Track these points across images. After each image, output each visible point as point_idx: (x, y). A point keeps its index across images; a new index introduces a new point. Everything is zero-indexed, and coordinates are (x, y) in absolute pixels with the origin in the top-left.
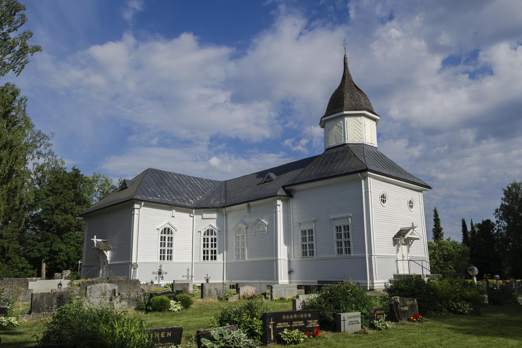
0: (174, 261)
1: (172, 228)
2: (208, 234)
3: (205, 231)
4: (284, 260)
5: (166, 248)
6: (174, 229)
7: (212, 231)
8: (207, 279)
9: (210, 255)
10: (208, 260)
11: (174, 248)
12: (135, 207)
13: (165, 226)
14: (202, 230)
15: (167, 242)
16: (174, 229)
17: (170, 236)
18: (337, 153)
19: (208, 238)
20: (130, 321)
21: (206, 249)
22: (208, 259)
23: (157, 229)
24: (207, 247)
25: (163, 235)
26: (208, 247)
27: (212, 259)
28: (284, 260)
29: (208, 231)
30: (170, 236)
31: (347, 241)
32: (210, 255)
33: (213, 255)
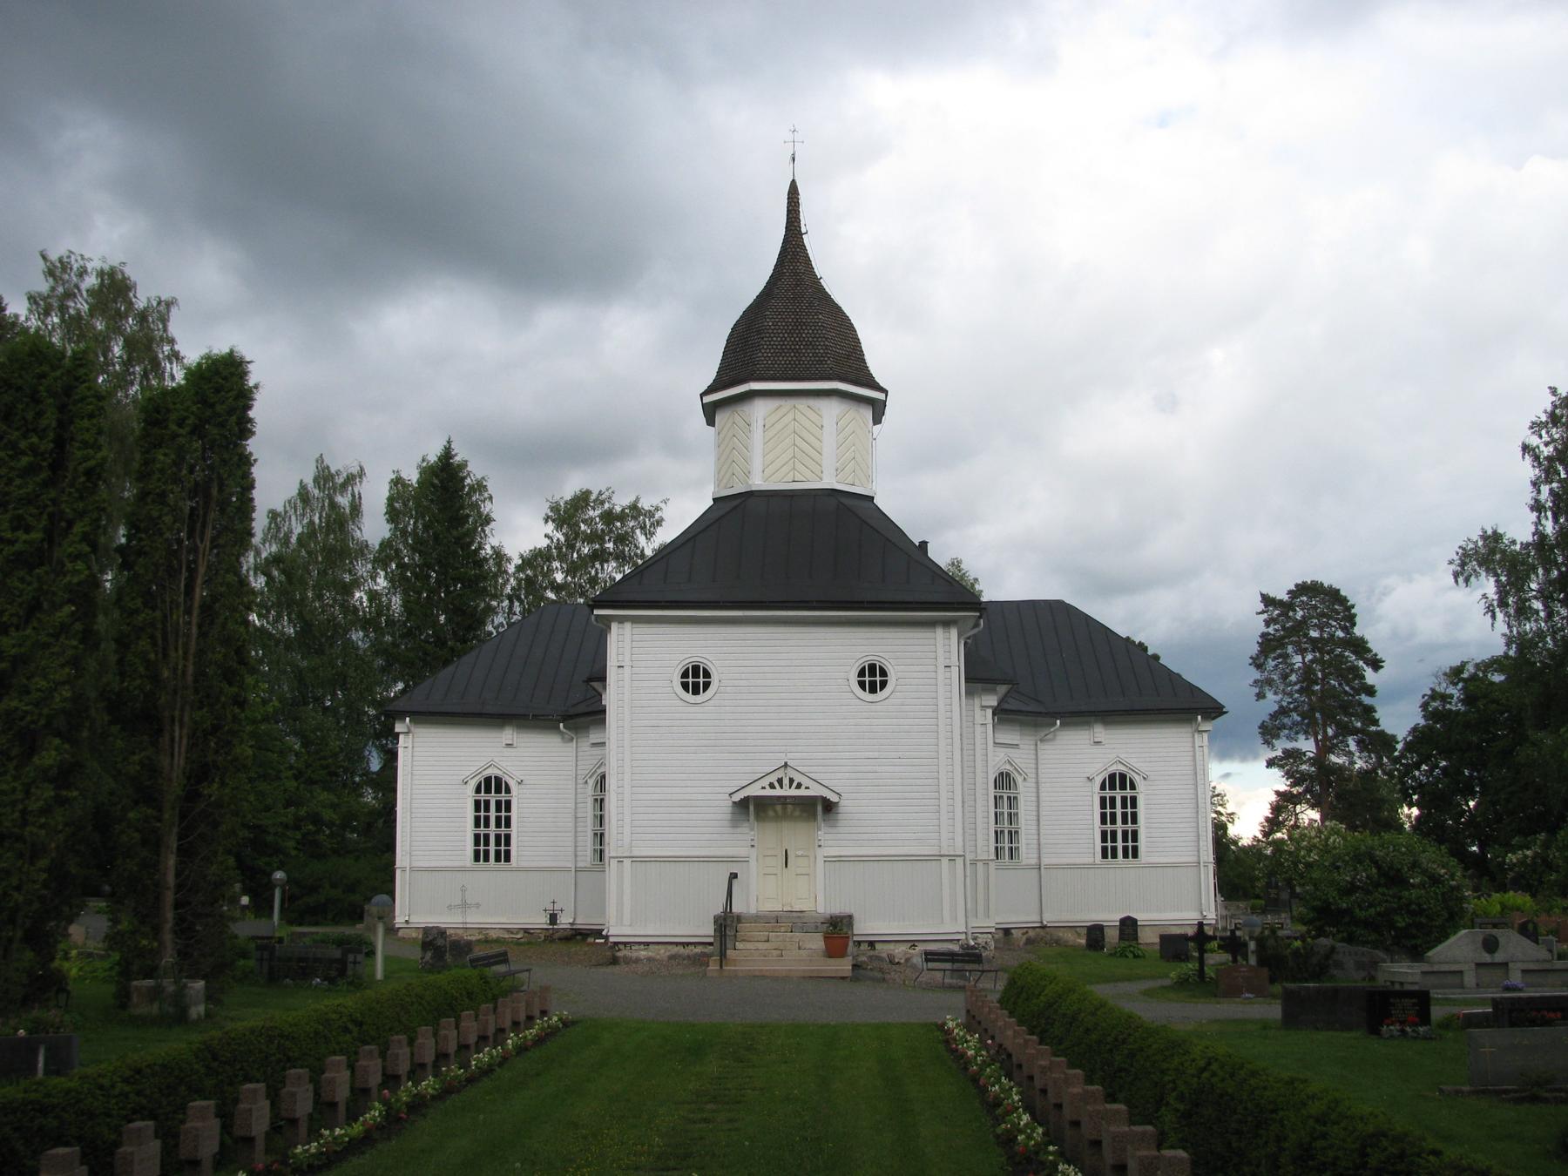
0: (1143, 862)
1: (1130, 772)
2: (488, 791)
3: (481, 782)
4: (634, 859)
5: (493, 830)
6: (1139, 775)
7: (499, 781)
8: (551, 915)
9: (492, 848)
10: (488, 861)
11: (469, 830)
12: (396, 730)
13: (1112, 769)
14: (591, 777)
15: (493, 814)
16: (1139, 775)
17: (1128, 793)
18: (868, 454)
19: (489, 801)
20: (1024, 995)
21: (1109, 827)
22: (487, 859)
23: (1088, 778)
24: (485, 827)
25: (1108, 793)
26: (487, 825)
27: (498, 859)
28: (634, 859)
29: (1112, 777)
30: (1128, 793)
31: (1012, 795)
32: (492, 848)
33: (1130, 844)
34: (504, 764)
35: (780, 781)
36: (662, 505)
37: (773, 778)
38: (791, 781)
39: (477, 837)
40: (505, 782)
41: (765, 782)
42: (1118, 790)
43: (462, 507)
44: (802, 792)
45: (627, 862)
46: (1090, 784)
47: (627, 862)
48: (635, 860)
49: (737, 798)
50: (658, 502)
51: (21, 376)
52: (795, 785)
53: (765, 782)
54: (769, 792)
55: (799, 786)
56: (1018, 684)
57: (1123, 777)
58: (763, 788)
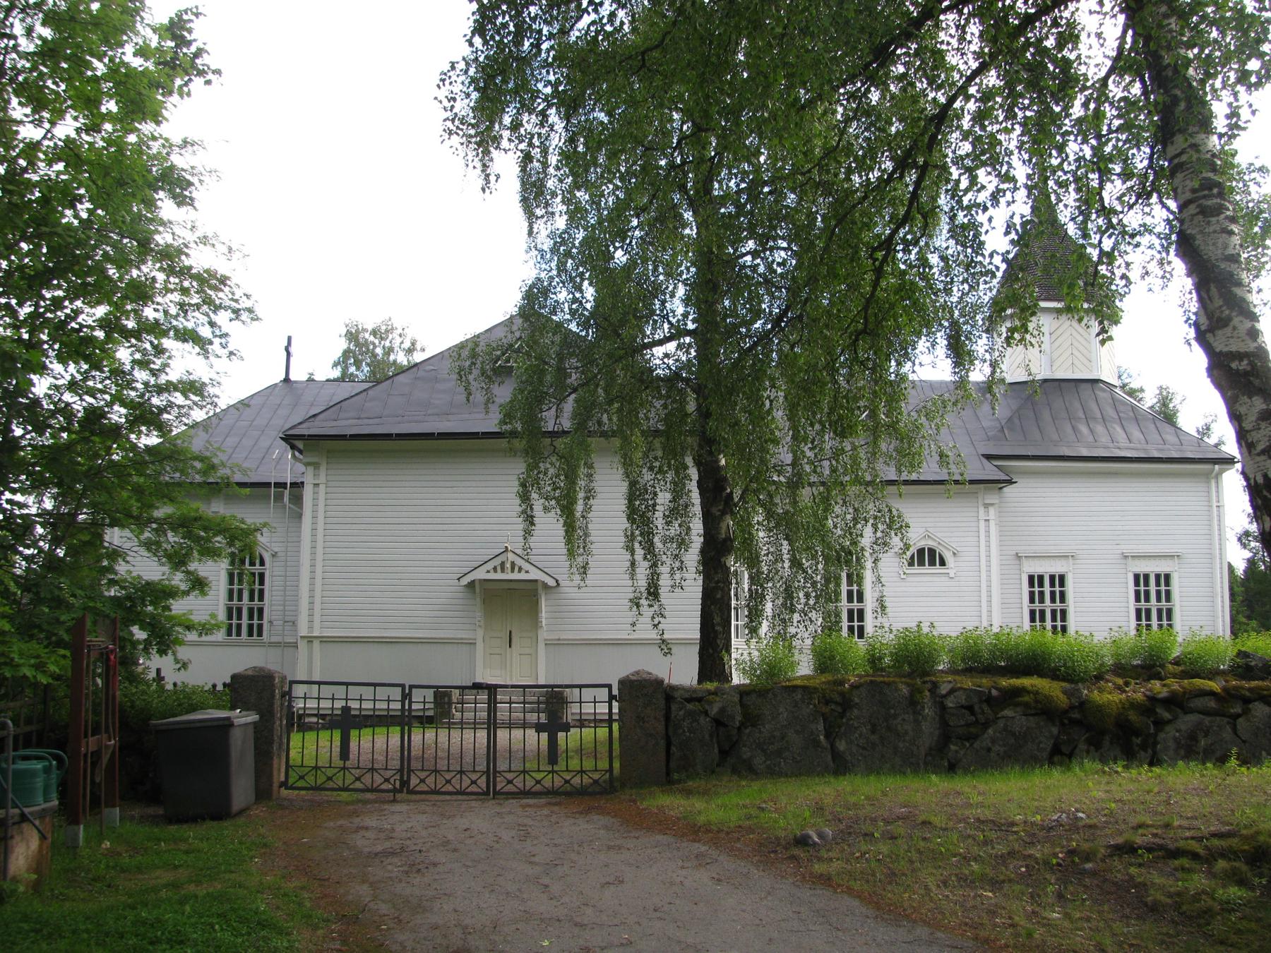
26: (1042, 601)
34: (939, 535)
35: (503, 564)
36: (192, 245)
37: (497, 562)
38: (513, 564)
39: (1138, 612)
40: (940, 555)
41: (490, 566)
42: (1038, 609)
43: (1232, 179)
44: (522, 576)
45: (316, 644)
46: (1124, 561)
47: (316, 644)
48: (324, 640)
49: (465, 581)
50: (191, 240)
51: (558, 283)
52: (517, 569)
53: (490, 566)
54: (492, 576)
55: (520, 569)
56: (226, 335)
57: (932, 552)
58: (488, 572)
